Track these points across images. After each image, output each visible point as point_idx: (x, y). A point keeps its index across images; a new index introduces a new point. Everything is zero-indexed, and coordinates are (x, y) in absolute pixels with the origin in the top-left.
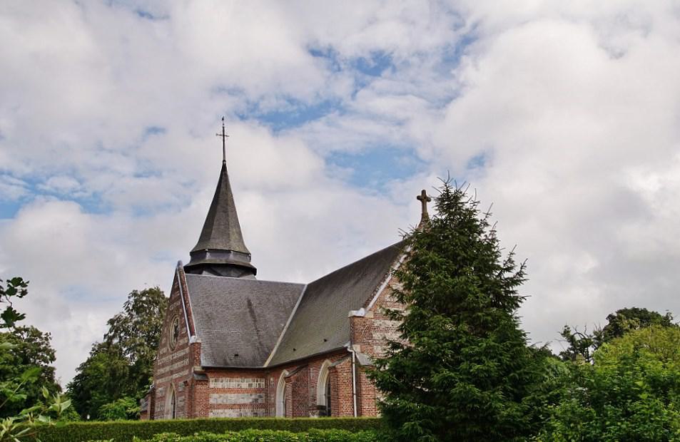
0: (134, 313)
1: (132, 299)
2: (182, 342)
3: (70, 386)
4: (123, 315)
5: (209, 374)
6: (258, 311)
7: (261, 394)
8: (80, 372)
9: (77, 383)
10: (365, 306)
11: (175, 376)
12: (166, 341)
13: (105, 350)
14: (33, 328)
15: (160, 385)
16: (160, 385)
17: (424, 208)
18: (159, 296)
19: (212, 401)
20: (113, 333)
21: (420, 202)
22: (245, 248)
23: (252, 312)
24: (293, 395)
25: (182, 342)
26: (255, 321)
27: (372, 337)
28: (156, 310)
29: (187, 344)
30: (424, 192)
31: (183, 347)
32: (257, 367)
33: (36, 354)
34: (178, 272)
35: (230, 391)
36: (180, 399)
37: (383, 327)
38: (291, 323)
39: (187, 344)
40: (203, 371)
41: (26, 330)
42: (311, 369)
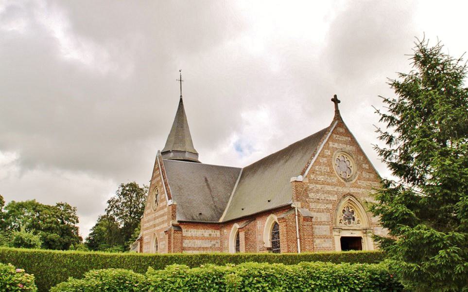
0: (122, 196)
1: (121, 189)
2: (161, 205)
3: (88, 239)
4: (115, 198)
5: (182, 226)
6: (212, 185)
7: (218, 241)
8: (92, 232)
9: (90, 237)
10: (303, 174)
11: (157, 228)
12: (150, 204)
13: (107, 221)
14: (66, 204)
15: (146, 235)
16: (146, 235)
17: (336, 107)
18: (136, 187)
19: (184, 245)
20: (110, 208)
21: (333, 103)
22: (195, 150)
23: (208, 185)
24: (245, 240)
25: (161, 205)
26: (211, 191)
27: (308, 196)
28: (134, 195)
29: (166, 206)
30: (335, 96)
31: (162, 208)
32: (215, 222)
33: (68, 219)
34: (158, 158)
35: (197, 238)
36: (161, 243)
37: (315, 189)
38: (235, 193)
39: (166, 206)
40: (178, 223)
41: (62, 205)
42: (258, 222)
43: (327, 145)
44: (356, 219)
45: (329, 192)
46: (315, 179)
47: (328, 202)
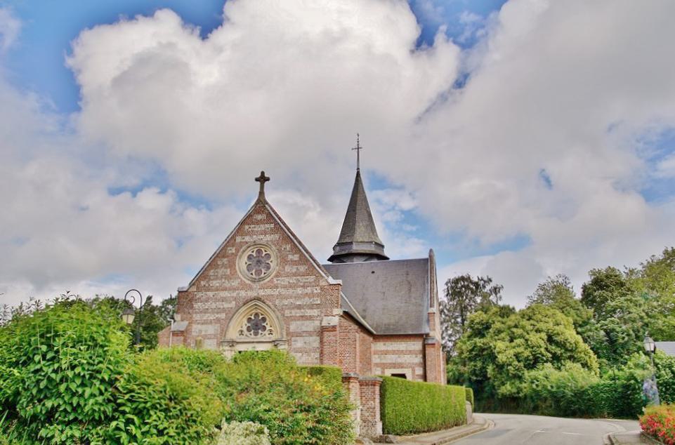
17: (262, 187)
27: (193, 307)
43: (233, 241)
44: (268, 328)
45: (224, 300)
46: (207, 285)
47: (219, 311)
